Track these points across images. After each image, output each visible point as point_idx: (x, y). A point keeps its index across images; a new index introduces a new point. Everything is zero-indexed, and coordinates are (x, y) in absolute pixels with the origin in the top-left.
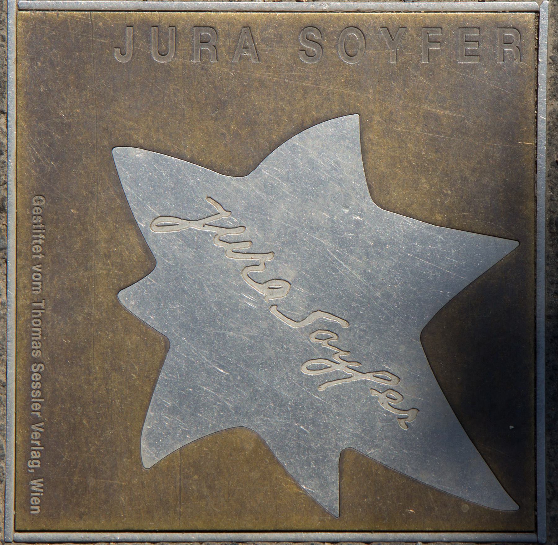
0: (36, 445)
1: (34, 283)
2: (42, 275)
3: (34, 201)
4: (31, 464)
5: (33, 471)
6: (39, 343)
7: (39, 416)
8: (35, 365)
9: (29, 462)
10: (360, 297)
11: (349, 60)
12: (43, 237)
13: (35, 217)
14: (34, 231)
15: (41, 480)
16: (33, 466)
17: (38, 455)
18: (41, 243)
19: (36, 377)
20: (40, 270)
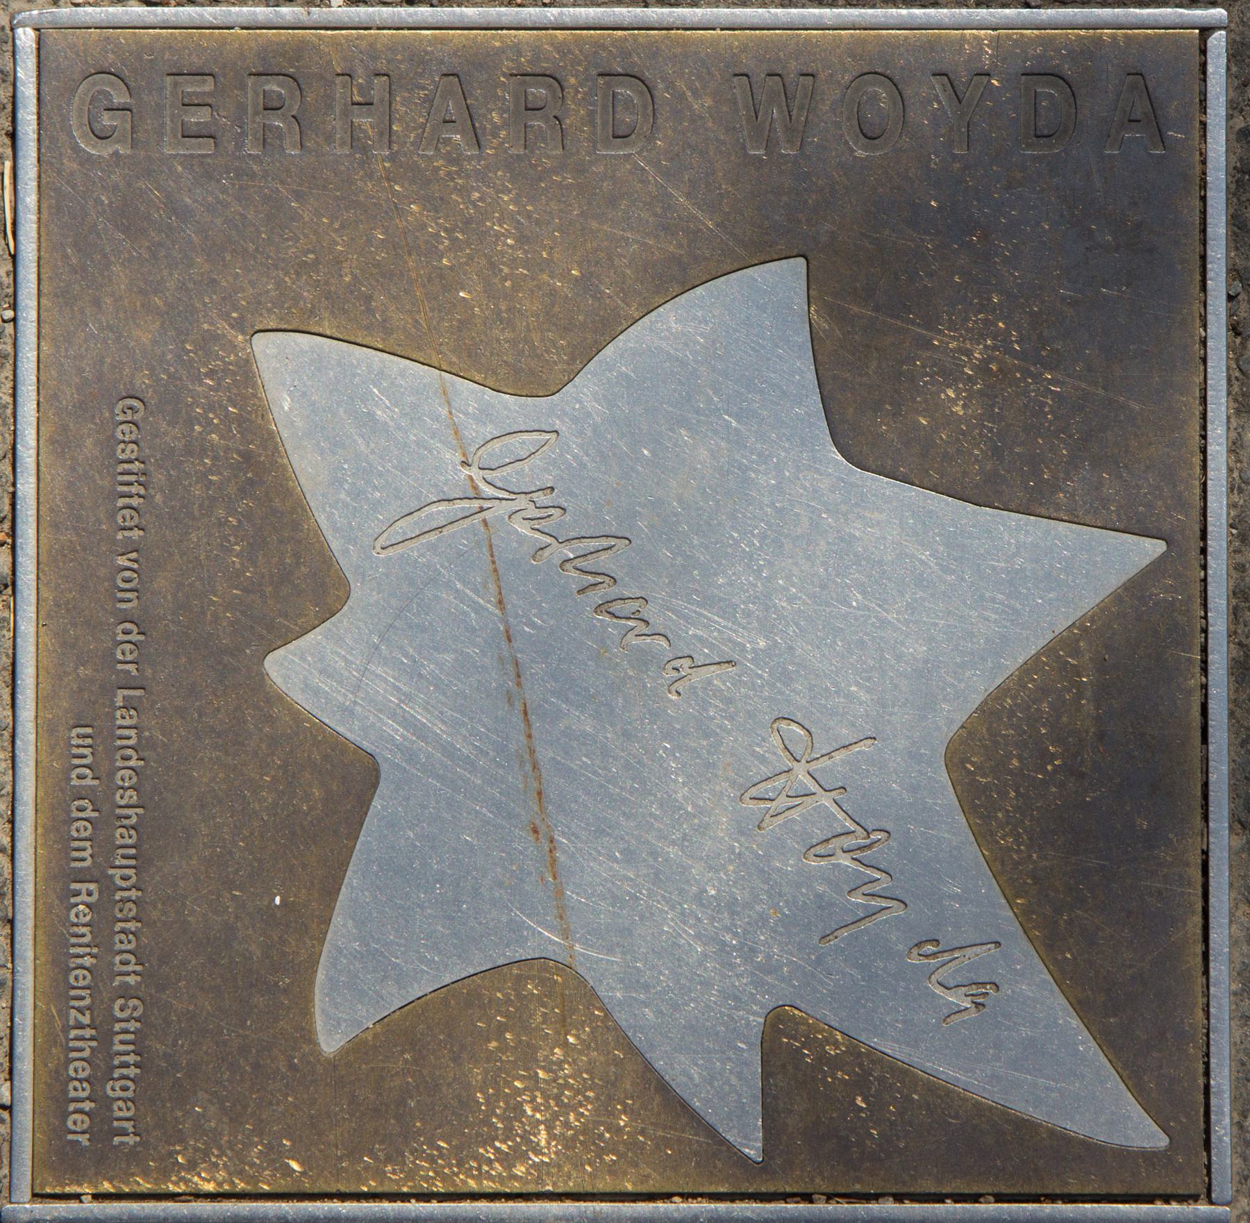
1: (120, 595)
4: (113, 1090)
6: (132, 832)
7: (135, 673)
11: (626, 145)
13: (122, 446)
14: (120, 478)
15: (134, 555)
17: (128, 1109)
18: (132, 1076)
20: (136, 566)
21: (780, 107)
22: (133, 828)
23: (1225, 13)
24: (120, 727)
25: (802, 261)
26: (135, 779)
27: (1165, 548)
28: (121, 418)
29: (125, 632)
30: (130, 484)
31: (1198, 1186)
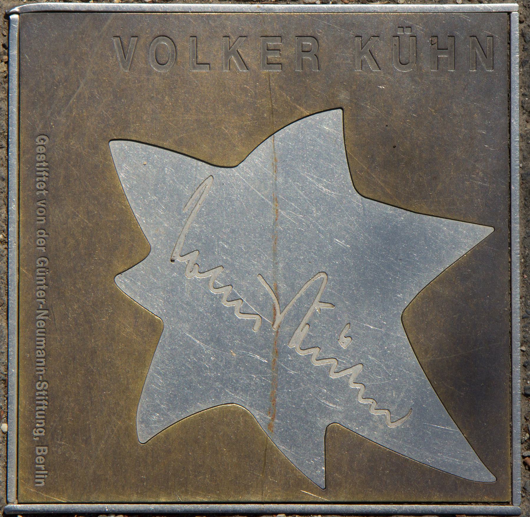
0: (40, 469)
2: (44, 429)
3: (38, 263)
5: (37, 439)
8: (39, 383)
9: (35, 430)
10: (366, 423)
12: (46, 403)
14: (38, 169)
16: (38, 434)
18: (44, 180)
19: (40, 459)
21: (478, 49)
22: (43, 349)
23: (518, 5)
24: (38, 358)
25: (340, 111)
26: (44, 460)
27: (493, 230)
28: (39, 265)
29: (40, 234)
30: (41, 400)
31: (509, 499)
